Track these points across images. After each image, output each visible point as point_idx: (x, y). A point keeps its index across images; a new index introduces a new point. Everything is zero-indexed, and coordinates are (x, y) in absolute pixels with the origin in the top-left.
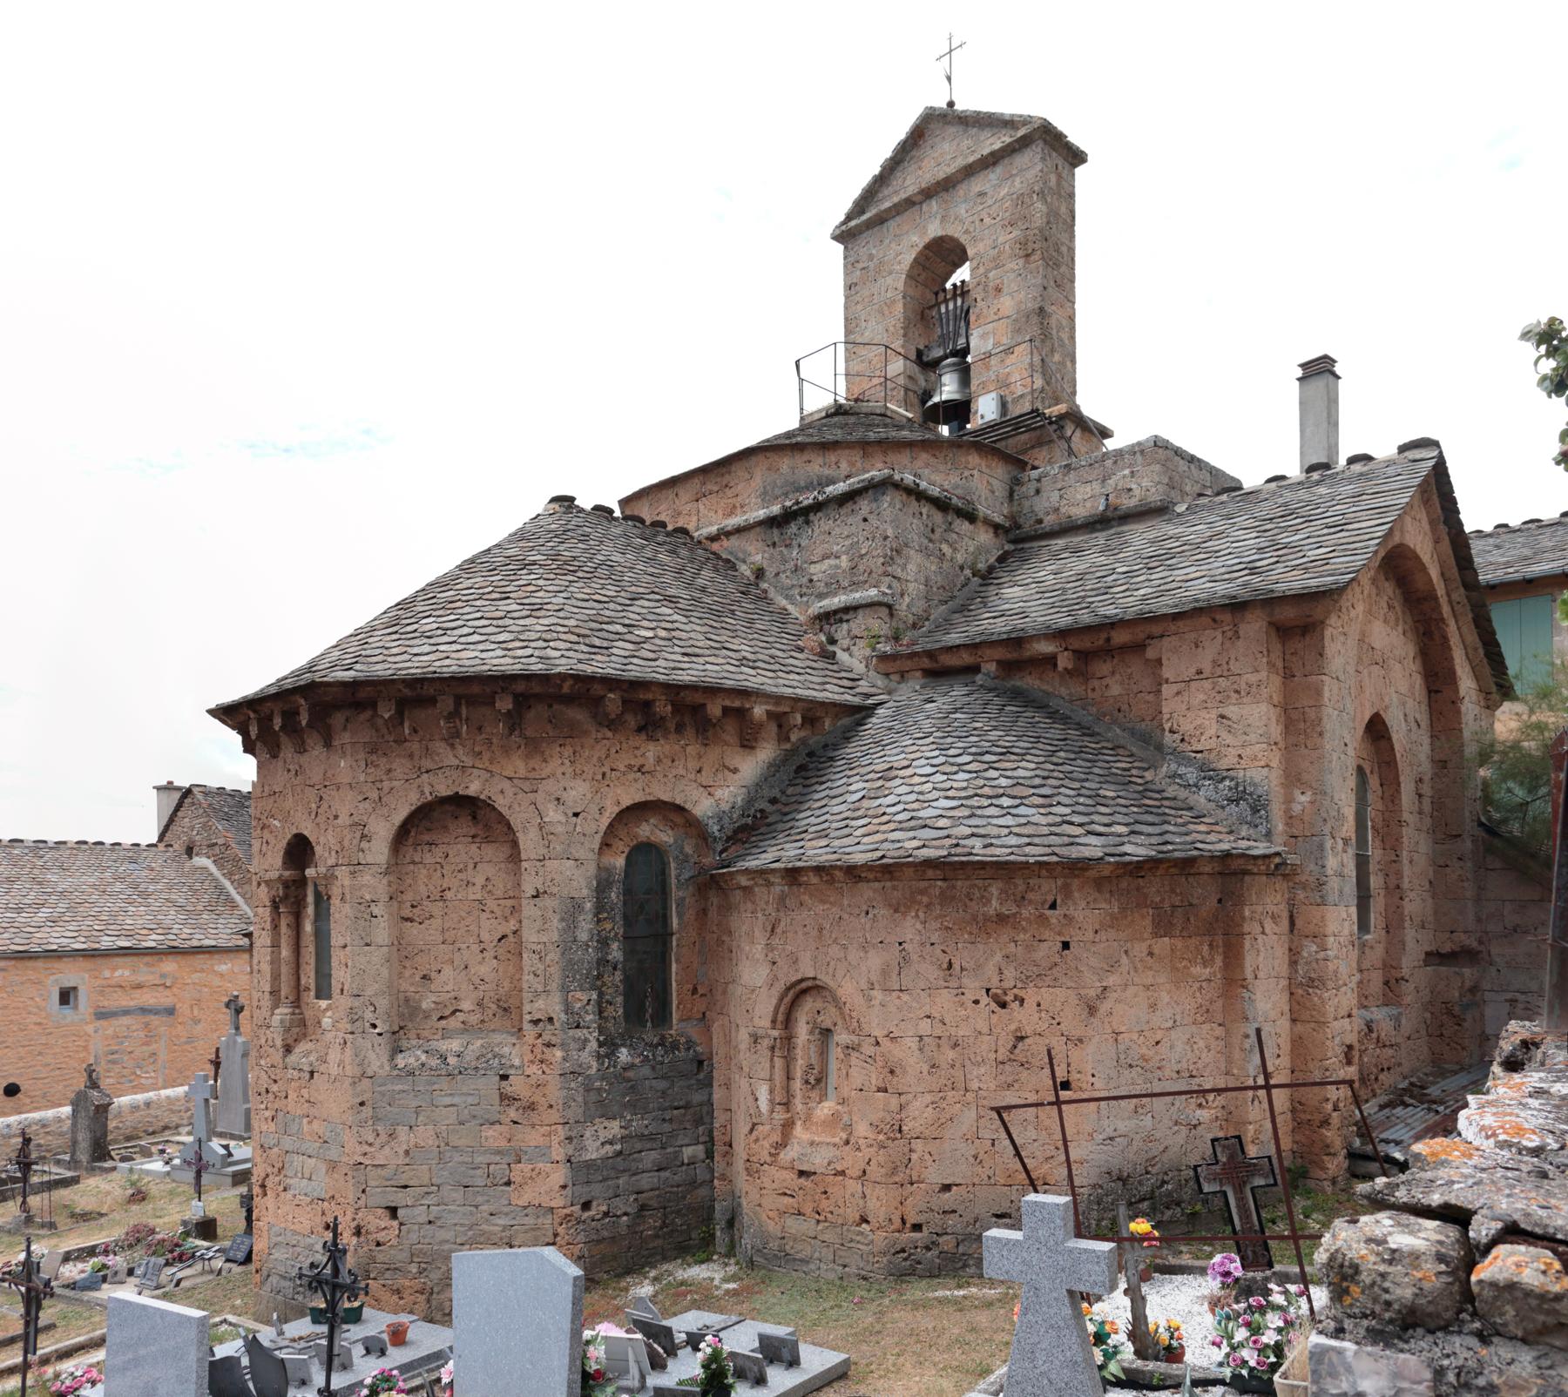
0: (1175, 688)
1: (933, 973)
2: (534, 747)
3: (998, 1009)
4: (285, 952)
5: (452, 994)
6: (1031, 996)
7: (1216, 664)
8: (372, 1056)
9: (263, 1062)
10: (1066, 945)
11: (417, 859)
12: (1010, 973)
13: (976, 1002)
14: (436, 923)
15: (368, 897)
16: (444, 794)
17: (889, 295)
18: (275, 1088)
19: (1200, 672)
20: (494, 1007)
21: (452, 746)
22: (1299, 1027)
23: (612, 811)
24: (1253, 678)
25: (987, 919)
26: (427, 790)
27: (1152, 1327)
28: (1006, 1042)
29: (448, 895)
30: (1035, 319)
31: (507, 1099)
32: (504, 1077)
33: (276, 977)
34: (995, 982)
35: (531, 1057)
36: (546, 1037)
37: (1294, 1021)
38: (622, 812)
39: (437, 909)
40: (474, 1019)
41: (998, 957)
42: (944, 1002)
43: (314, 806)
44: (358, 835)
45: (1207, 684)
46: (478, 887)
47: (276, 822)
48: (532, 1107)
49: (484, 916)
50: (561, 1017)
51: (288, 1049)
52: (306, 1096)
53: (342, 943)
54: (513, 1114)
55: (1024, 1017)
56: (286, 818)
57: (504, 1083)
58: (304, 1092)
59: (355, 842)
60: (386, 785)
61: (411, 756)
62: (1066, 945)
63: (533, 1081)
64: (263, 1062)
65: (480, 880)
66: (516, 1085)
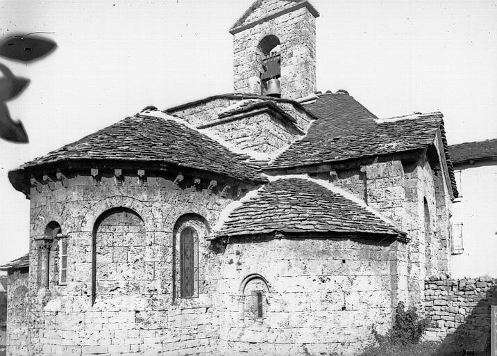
0: (371, 181)
1: (300, 271)
2: (151, 191)
3: (321, 283)
4: (44, 267)
5: (116, 282)
6: (333, 278)
7: (384, 173)
8: (84, 304)
9: (32, 310)
10: (344, 261)
11: (103, 231)
12: (325, 271)
13: (315, 280)
14: (110, 255)
15: (85, 244)
16: (116, 206)
17: (251, 53)
18: (38, 320)
19: (379, 176)
20: (133, 286)
21: (119, 189)
22: (411, 293)
23: (178, 216)
24: (397, 178)
25: (319, 252)
26: (109, 205)
27: (439, 340)
28: (324, 293)
29: (115, 244)
30: (304, 65)
31: (138, 320)
32: (137, 312)
33: (39, 277)
34: (321, 274)
35: (148, 304)
36: (154, 296)
37: (410, 291)
38: (181, 217)
39: (110, 250)
40: (124, 291)
41: (321, 266)
42: (303, 280)
43: (61, 210)
44: (81, 221)
45: (382, 180)
46: (127, 241)
47: (42, 218)
48: (148, 323)
49: (129, 253)
50: (160, 290)
51: (44, 304)
52: (54, 321)
53: (73, 261)
54: (140, 325)
55: (329, 285)
56: (47, 215)
57: (137, 314)
58: (53, 320)
59: (80, 223)
60: (92, 202)
61: (102, 192)
62: (344, 261)
63: (148, 313)
64: (32, 310)
65: (128, 239)
66: (142, 315)
